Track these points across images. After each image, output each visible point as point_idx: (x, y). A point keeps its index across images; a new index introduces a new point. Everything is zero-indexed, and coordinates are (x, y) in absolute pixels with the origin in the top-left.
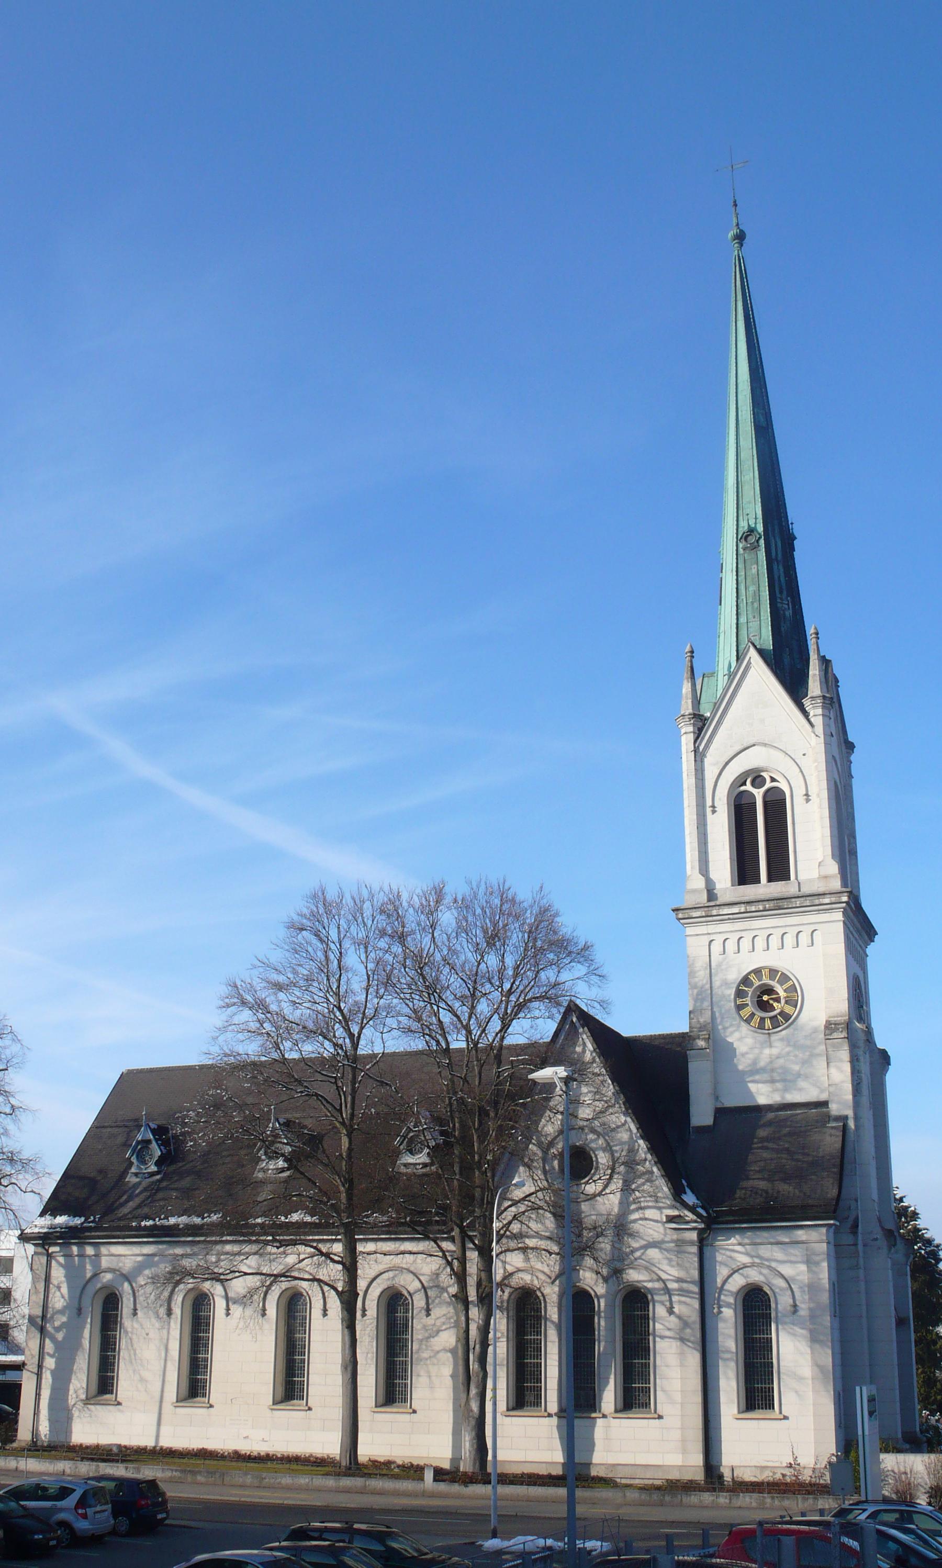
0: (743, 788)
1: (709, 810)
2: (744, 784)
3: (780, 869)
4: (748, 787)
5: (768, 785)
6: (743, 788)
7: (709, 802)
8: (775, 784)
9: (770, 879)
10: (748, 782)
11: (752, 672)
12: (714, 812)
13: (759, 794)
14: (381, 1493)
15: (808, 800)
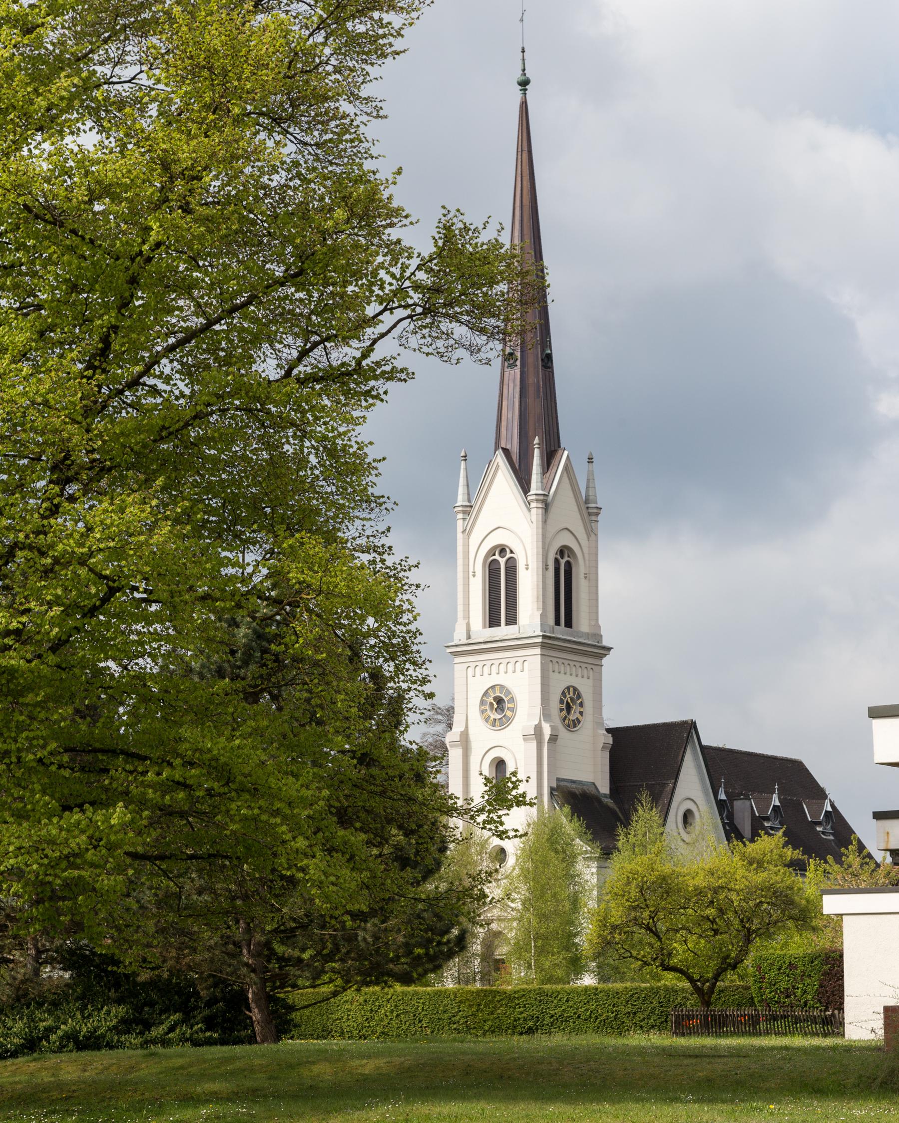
0: (494, 557)
1: (471, 576)
2: (494, 555)
3: (512, 620)
4: (497, 557)
5: (508, 555)
6: (494, 557)
7: (471, 570)
8: (512, 555)
9: (507, 625)
10: (497, 553)
11: (500, 473)
12: (474, 576)
13: (502, 561)
14: (467, 585)
15: (527, 569)
